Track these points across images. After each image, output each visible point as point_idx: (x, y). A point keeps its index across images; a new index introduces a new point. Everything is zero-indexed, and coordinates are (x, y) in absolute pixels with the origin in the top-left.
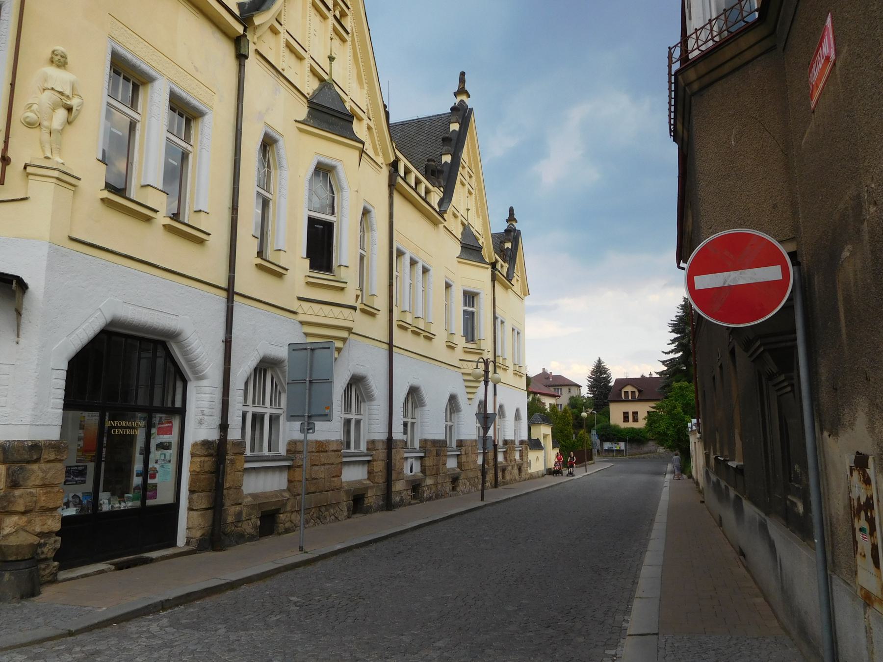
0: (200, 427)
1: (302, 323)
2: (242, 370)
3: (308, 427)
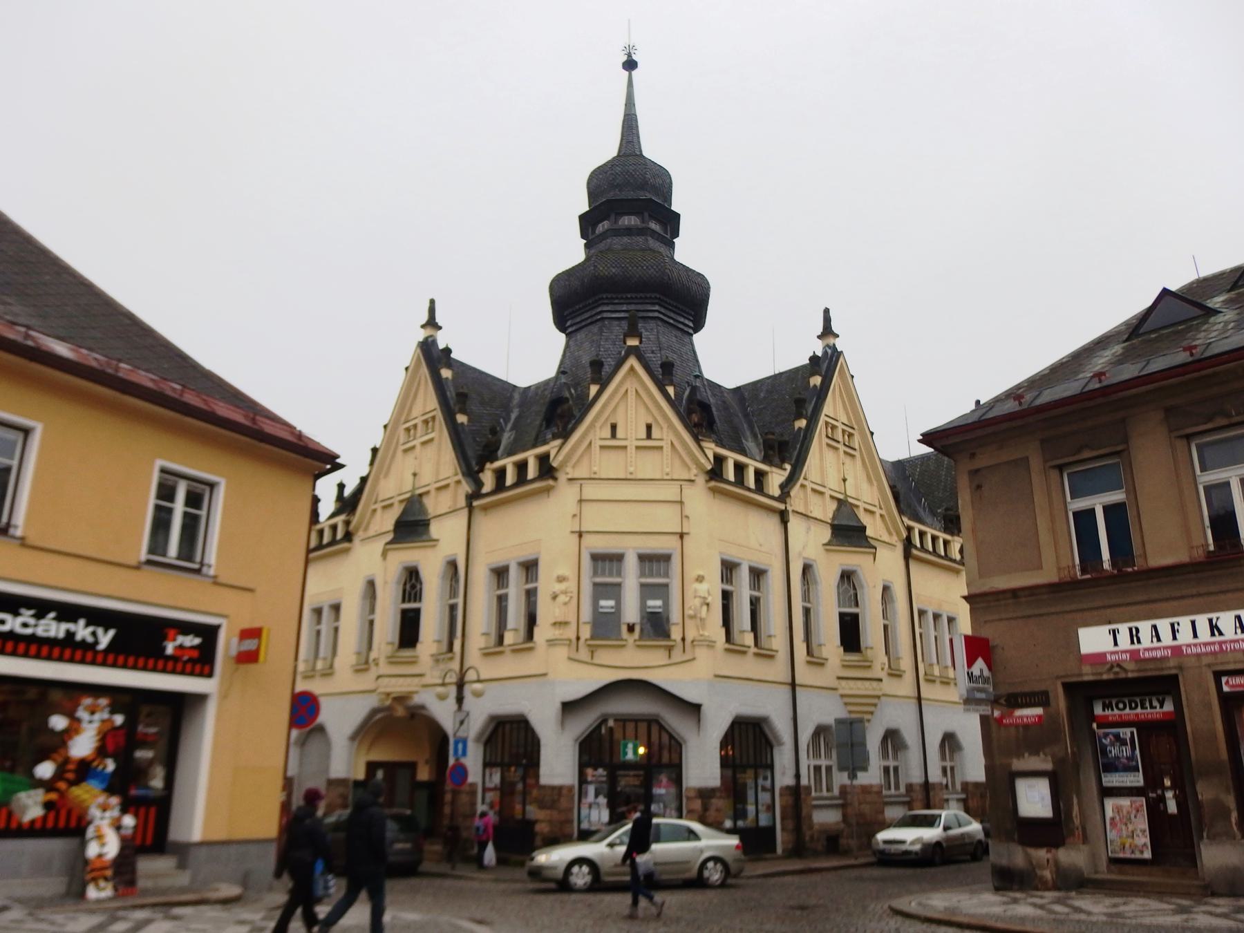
0: (784, 778)
1: (842, 696)
2: (805, 736)
3: (853, 776)
